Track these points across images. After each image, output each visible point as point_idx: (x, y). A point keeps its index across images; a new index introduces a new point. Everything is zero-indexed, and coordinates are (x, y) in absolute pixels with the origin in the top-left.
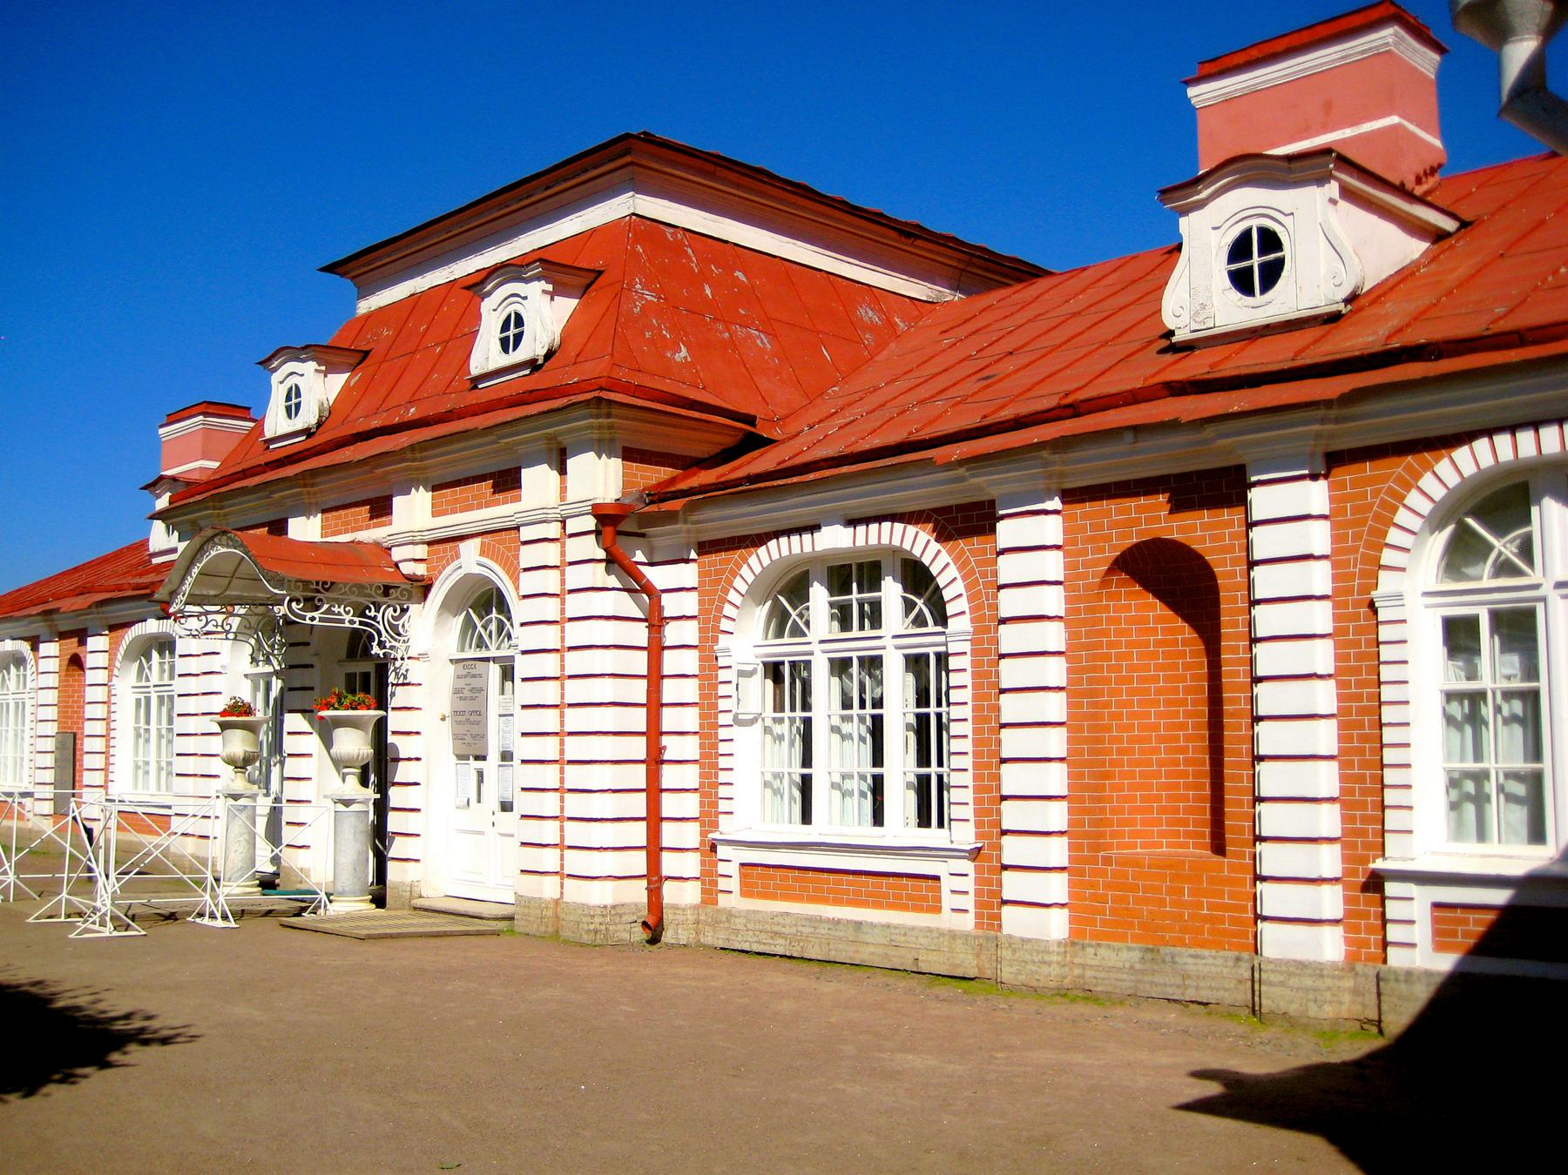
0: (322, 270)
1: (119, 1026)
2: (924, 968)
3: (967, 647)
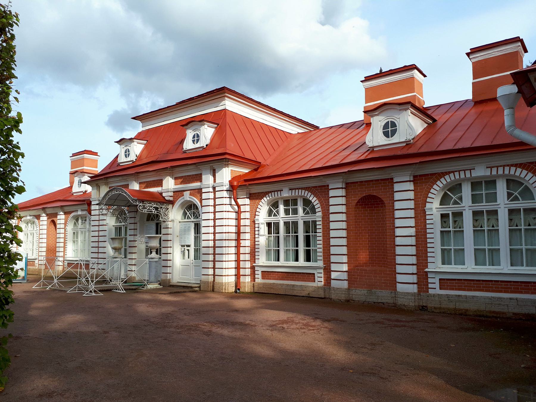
0: (132, 118)
1: (440, 382)
3: (321, 219)
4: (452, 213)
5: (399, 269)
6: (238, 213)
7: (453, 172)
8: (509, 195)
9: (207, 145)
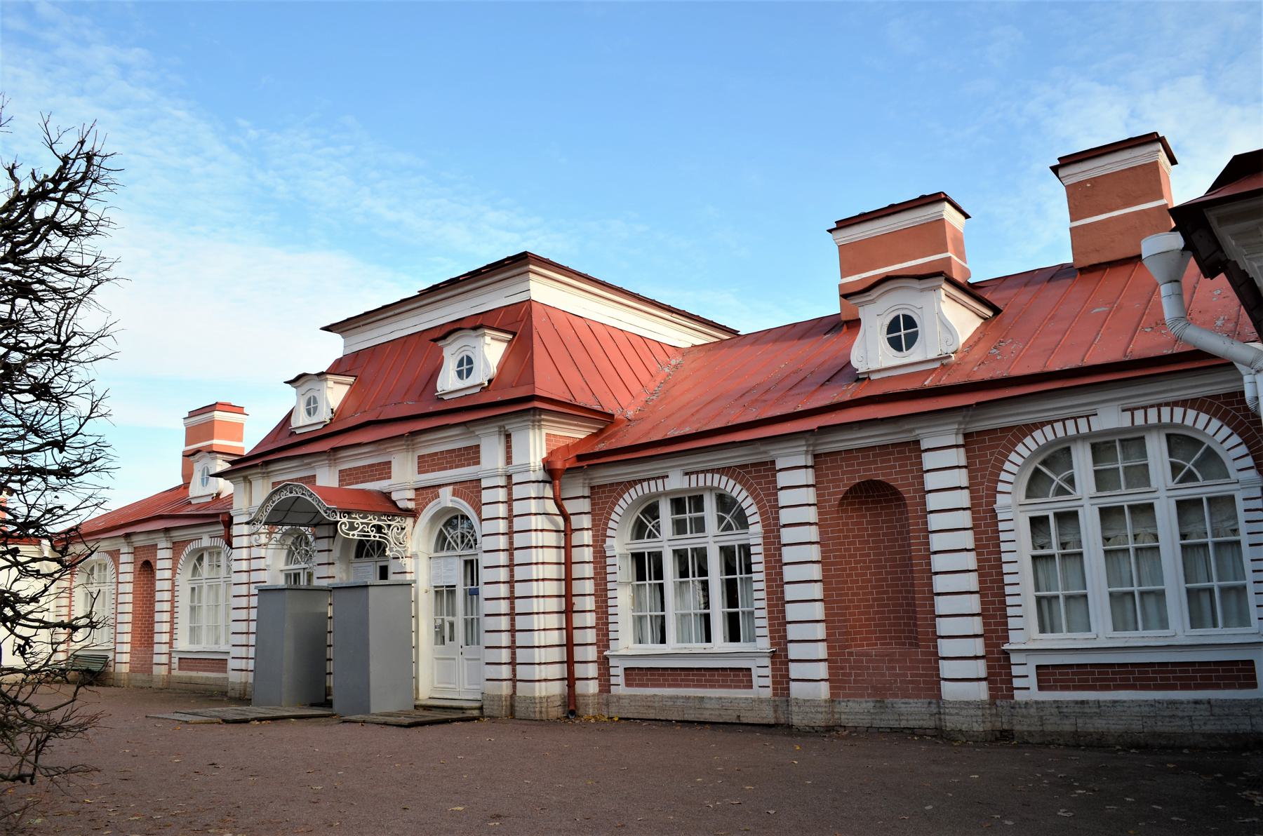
2: (744, 720)
3: (760, 541)
4: (1056, 514)
5: (945, 648)
6: (568, 532)
7: (1051, 423)
8: (1175, 468)
9: (490, 381)
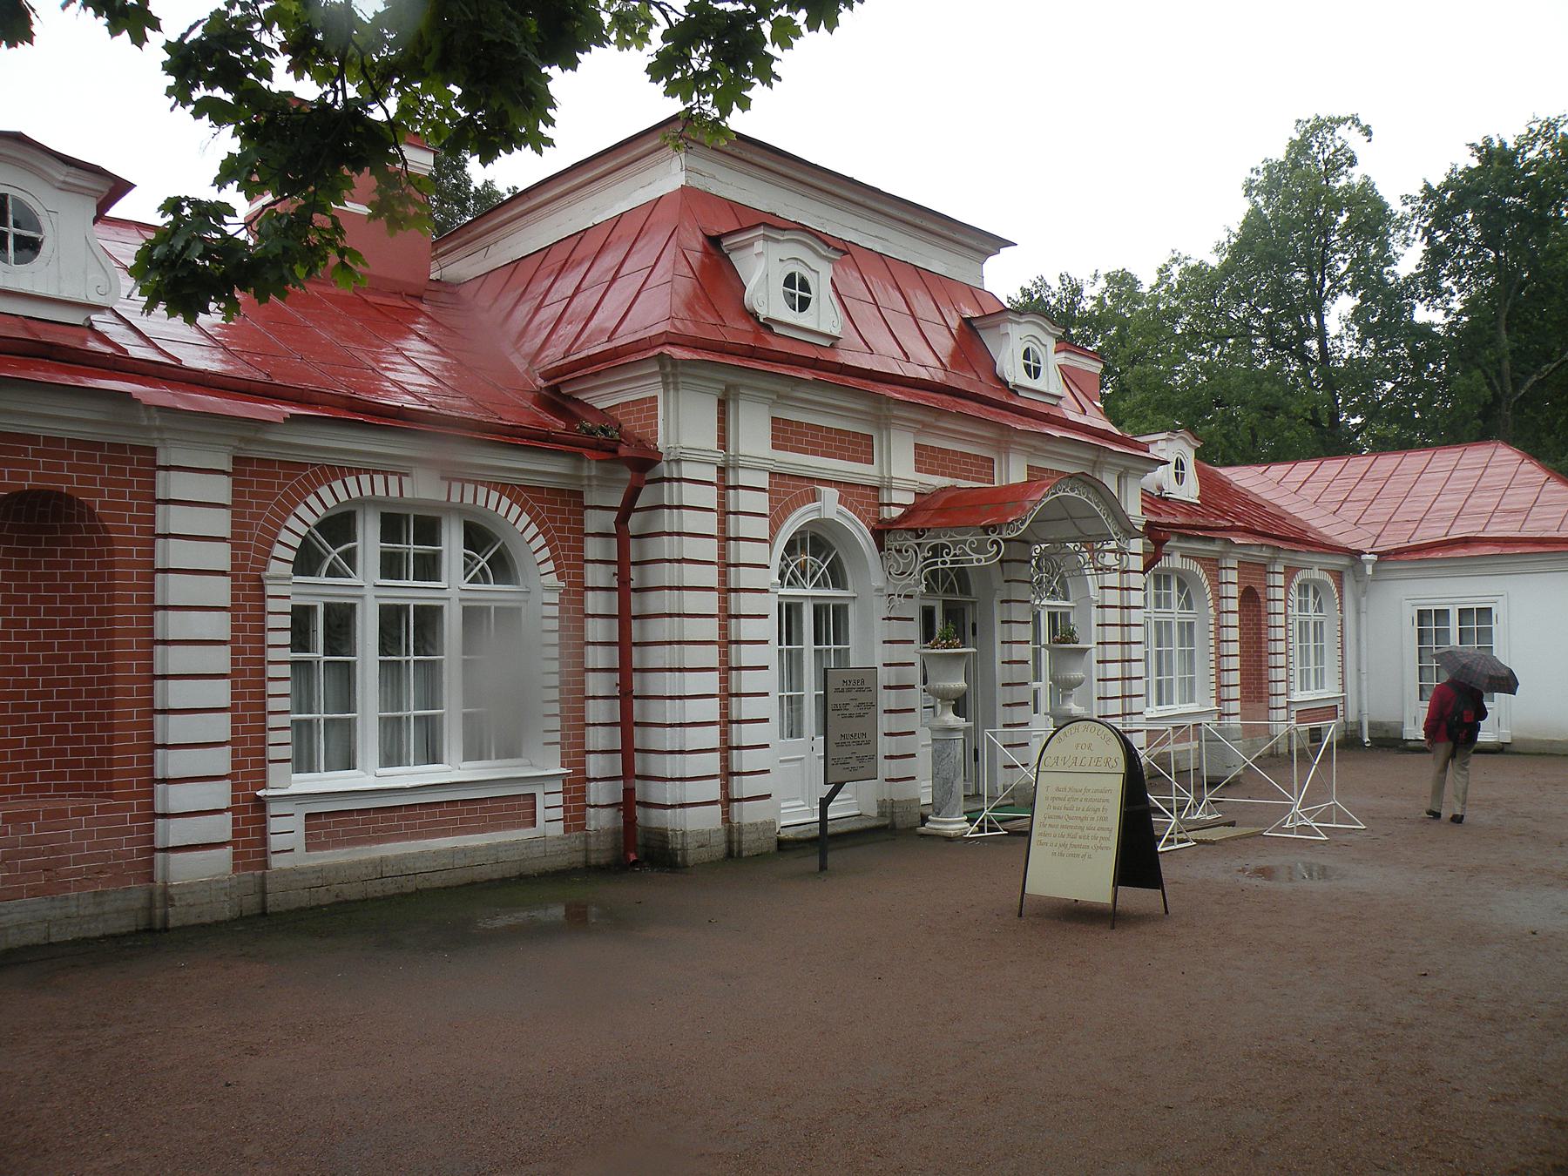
4: (327, 605)
